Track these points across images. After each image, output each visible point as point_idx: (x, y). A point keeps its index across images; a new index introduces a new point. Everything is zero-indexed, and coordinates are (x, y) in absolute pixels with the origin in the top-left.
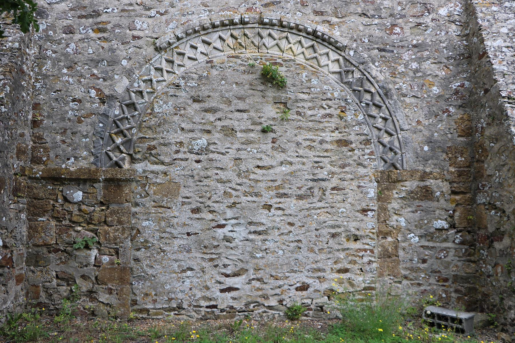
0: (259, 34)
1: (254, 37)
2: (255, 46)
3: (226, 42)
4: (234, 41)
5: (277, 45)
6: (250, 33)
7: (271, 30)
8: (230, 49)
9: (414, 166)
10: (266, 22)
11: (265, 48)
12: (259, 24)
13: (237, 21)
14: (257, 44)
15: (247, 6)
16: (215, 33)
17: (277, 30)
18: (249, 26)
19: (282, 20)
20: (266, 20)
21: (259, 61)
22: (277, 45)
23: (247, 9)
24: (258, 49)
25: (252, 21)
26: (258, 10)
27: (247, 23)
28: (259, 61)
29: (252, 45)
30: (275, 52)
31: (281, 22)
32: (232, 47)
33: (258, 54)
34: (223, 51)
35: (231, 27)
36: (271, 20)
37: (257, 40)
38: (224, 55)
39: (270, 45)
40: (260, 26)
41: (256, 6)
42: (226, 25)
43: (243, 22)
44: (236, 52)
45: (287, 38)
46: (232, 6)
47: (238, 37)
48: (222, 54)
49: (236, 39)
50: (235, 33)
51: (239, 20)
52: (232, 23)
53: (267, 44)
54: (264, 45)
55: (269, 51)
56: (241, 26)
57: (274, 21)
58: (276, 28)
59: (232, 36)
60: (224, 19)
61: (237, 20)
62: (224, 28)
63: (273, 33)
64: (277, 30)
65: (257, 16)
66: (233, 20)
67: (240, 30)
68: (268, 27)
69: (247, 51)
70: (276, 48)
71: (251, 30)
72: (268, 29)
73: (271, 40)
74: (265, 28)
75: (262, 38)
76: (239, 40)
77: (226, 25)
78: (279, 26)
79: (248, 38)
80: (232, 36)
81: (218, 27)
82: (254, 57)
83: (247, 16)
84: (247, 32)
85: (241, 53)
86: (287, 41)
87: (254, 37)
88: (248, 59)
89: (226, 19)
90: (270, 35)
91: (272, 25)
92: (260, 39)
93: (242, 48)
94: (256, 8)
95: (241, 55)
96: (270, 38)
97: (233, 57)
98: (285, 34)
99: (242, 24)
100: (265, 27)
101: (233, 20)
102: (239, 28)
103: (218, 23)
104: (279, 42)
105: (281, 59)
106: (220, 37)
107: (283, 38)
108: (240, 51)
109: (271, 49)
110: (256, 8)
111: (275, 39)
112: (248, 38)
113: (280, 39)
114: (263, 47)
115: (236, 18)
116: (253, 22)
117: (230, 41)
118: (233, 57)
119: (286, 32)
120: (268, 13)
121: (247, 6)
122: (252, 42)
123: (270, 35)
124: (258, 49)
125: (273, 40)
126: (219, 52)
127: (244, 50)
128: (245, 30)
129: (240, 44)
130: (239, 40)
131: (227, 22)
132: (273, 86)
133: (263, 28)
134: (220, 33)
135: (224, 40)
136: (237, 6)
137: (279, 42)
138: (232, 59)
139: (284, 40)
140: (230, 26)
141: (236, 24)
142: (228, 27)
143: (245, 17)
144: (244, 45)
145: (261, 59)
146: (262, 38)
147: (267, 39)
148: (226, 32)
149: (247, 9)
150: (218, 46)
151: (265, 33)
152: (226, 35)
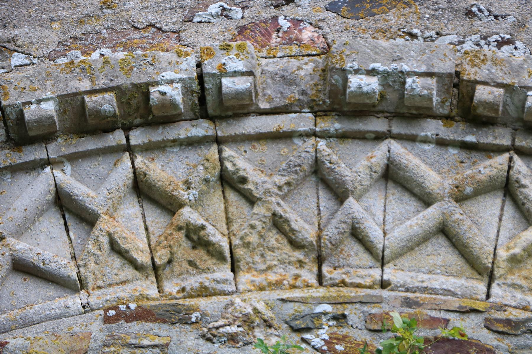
0: (320, 174)
1: (288, 191)
2: (295, 245)
3: (104, 224)
4: (157, 220)
5: (444, 231)
6: (262, 168)
7: (397, 149)
8: (129, 272)
9: (210, 262)
10: (360, 93)
11: (365, 258)
12: (319, 112)
13: (175, 93)
14: (308, 232)
15: (237, 13)
16: (24, 179)
17: (442, 143)
18: (253, 125)
19: (470, 73)
20: (362, 83)
21: (324, 333)
22: (444, 231)
23: (241, 30)
24: (320, 261)
25: (270, 95)
26: (307, 34)
27: (240, 107)
28: (324, 333)
29: (273, 238)
30: (437, 274)
31: (458, 86)
32: (143, 258)
33: (321, 292)
34: (77, 286)
35: (137, 137)
36: (394, 80)
37: (305, 213)
38: (86, 308)
39: (399, 234)
40: (324, 125)
41: (299, 13)
42: (103, 125)
43: (209, 102)
44: (171, 287)
45: (508, 188)
46: (143, 19)
47: (184, 195)
48: (75, 301)
49: (169, 205)
50: (163, 171)
51: (187, 91)
52: (141, 110)
53: (374, 231)
54: (357, 234)
55: (390, 273)
56: (201, 129)
57: (415, 85)
58: (432, 128)
59: (142, 189)
60: (85, 85)
61: (170, 84)
62: (90, 144)
63: (414, 161)
64: (442, 143)
65: (306, 69)
66: (143, 90)
67: (193, 156)
68: (378, 125)
69: (245, 278)
70: (441, 253)
71: (269, 152)
72: (379, 137)
73: (399, 204)
74: (360, 137)
75: (339, 193)
76: (188, 215)
77: (103, 125)
78: (447, 118)
79: (251, 200)
80: (142, 189)
81: (45, 134)
82: (290, 309)
83: (236, 64)
84: (240, 161)
85: (204, 292)
86: (509, 210)
87: (288, 191)
88: (247, 321)
89: (101, 82)
90: (391, 175)
91: (400, 110)
92: (326, 201)
93: (210, 262)
94: (296, 22)
95: (202, 303)
96: (395, 193)
97: (143, 315)
98: (492, 167)
99: (205, 116)
100: (360, 126)
101: (143, 90)
102: (192, 143)
103: (49, 108)
104: (457, 213)
105: (475, 320)
106: (63, 203)
107: (483, 189)
108: (193, 282)
109: (406, 261)
110: (296, 22)
111: (426, 200)
112: (251, 200)
113: (461, 198)
114: (353, 248)
115: (169, 75)
116: (278, 102)
117: (132, 224)
118: (143, 315)
119: (500, 150)
120: (365, 43)
121: (237, 13)
122: (278, 223)
123: (391, 175)
124: (320, 261)
125: (412, 204)
126: (51, 291)
127: (224, 272)
128: (228, 152)
129: (196, 238)
130: (188, 215)
131: (108, 103)
132: (258, 310)
133: (343, 136)
134: (66, 177)
135: (87, 219)
136: (177, 17)
137: (457, 213)
138: (135, 327)
139: (491, 207)
140: (127, 129)
141: (167, 117)
142: (118, 138)
143: (223, 72)
144: (217, 236)
145: (340, 319)
146: (339, 193)
147: (376, 200)
148: (100, 166)
149: (241, 30)
150: (47, 255)
151: (356, 164)
152: (101, 184)
